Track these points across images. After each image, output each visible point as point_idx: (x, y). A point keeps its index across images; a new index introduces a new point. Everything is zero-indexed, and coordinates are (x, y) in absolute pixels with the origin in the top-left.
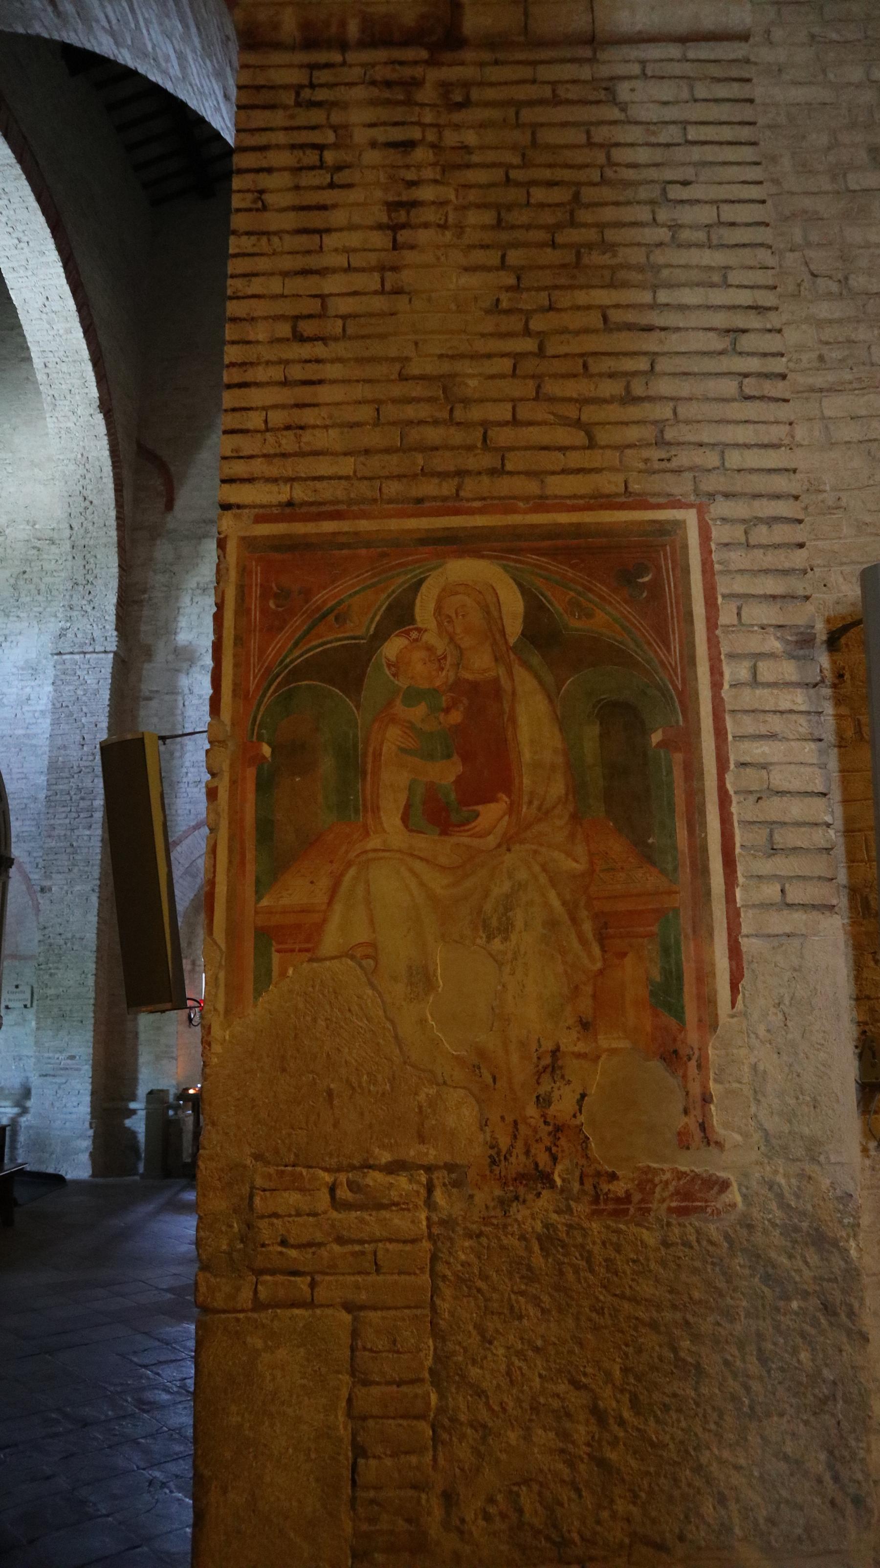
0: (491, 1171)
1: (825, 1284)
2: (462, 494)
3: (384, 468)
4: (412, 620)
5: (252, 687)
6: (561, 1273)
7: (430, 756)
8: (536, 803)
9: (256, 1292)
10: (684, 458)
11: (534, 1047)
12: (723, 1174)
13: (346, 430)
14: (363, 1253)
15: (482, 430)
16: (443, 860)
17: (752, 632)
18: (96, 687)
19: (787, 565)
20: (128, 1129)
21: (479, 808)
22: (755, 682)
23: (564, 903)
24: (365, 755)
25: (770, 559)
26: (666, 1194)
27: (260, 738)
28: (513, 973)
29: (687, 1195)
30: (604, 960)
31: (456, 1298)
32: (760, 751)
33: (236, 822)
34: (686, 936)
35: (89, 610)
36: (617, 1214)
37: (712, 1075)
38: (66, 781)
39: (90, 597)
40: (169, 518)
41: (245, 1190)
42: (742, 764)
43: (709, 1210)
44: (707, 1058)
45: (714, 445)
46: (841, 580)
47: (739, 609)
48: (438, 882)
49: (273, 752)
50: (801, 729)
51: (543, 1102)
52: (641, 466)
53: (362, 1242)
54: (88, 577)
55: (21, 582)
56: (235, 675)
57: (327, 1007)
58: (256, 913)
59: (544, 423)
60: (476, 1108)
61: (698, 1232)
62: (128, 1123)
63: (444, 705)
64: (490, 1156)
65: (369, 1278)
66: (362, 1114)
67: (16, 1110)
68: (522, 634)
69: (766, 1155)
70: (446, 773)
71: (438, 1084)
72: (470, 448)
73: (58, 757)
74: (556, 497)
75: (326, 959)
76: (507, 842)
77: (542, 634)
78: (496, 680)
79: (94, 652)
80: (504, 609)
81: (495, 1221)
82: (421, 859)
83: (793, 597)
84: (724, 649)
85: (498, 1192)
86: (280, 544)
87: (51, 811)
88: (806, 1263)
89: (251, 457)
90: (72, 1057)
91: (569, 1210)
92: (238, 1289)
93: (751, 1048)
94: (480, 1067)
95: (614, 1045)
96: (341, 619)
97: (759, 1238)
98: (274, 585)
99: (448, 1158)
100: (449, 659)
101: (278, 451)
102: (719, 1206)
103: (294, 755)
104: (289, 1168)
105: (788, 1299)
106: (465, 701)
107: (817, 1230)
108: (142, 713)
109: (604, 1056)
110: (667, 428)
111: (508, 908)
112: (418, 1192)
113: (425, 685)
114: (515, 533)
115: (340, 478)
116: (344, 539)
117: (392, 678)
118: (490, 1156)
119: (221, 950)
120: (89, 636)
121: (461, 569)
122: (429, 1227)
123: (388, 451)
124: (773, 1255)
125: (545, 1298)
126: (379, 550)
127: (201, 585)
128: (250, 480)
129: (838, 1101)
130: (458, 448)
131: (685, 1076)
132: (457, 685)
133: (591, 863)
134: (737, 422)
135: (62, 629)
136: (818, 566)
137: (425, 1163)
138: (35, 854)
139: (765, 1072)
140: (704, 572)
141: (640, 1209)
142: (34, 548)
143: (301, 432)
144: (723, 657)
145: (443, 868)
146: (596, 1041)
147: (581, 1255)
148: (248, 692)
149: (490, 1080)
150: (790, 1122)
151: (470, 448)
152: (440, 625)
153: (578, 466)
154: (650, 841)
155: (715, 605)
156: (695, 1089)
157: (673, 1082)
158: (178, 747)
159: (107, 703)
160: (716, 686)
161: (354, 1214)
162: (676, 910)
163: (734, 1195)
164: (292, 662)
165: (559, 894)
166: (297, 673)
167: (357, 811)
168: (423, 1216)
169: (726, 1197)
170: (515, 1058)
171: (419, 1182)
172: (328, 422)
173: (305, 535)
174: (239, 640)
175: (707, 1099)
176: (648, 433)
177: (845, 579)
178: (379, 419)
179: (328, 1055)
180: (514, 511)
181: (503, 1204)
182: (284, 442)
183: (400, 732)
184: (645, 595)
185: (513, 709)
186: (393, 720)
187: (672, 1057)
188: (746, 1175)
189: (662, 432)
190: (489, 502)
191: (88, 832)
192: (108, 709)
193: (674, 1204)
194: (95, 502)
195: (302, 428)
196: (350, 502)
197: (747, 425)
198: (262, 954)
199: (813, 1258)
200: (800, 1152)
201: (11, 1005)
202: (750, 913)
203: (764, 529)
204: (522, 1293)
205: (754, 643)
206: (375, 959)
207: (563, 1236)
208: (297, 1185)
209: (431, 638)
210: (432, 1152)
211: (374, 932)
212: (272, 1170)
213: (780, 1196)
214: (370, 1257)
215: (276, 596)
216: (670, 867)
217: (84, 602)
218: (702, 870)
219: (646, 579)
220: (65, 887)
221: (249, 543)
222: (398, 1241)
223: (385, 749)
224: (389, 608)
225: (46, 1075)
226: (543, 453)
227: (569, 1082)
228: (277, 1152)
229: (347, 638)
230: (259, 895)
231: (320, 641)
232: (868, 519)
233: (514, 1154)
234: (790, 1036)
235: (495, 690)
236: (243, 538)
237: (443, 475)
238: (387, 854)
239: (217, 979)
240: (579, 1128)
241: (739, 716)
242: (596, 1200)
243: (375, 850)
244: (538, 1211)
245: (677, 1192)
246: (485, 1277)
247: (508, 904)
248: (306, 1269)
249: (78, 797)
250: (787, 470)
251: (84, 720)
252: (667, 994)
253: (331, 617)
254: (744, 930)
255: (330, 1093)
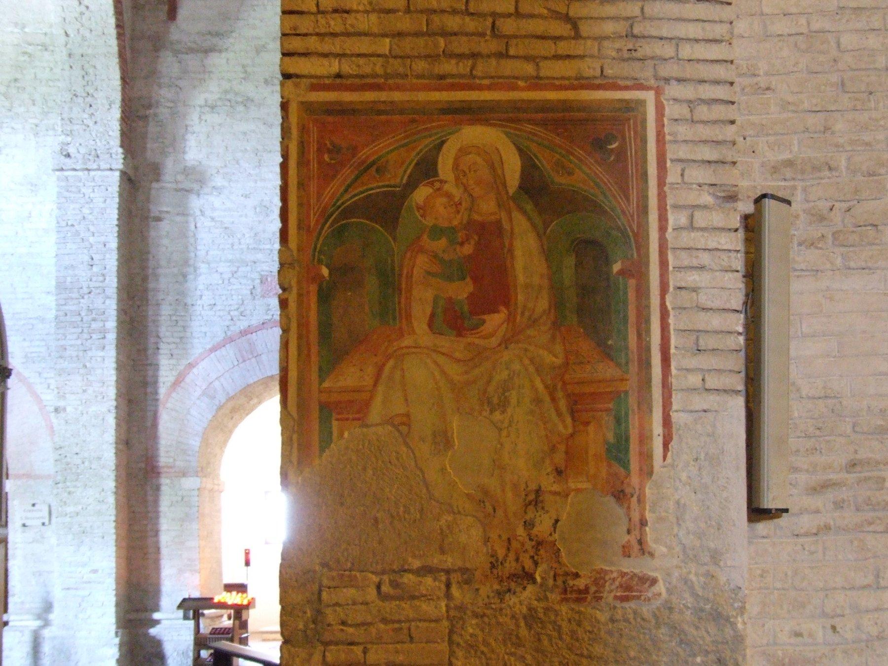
0: (492, 573)
1: (719, 646)
2: (474, 72)
3: (413, 49)
4: (436, 174)
5: (312, 224)
6: (539, 640)
7: (450, 278)
8: (527, 314)
9: (324, 656)
10: (646, 49)
11: (523, 486)
12: (653, 574)
13: (382, 15)
14: (401, 629)
15: (490, 20)
16: (457, 355)
17: (691, 189)
18: (103, 205)
19: (720, 138)
20: (154, 637)
21: (485, 317)
22: (691, 227)
23: (546, 387)
24: (400, 275)
25: (706, 132)
26: (613, 587)
27: (320, 261)
28: (508, 436)
29: (629, 588)
30: (574, 427)
31: (466, 658)
32: (693, 278)
33: (303, 325)
34: (633, 410)
35: (91, 124)
36: (578, 600)
37: (647, 507)
38: (76, 302)
39: (92, 111)
40: (173, 28)
41: (316, 587)
42: (679, 288)
43: (643, 598)
44: (645, 495)
45: (671, 39)
46: (766, 148)
47: (683, 170)
48: (454, 371)
49: (330, 274)
50: (723, 263)
51: (529, 525)
52: (614, 54)
53: (399, 621)
54: (88, 89)
55: (14, 91)
56: (299, 213)
57: (374, 459)
58: (320, 392)
59: (540, 16)
60: (481, 530)
61: (635, 612)
62: (153, 631)
63: (460, 240)
64: (491, 563)
65: (405, 646)
66: (399, 534)
67: (38, 623)
68: (520, 187)
69: (683, 561)
70: (461, 291)
71: (454, 513)
72: (482, 35)
73: (65, 277)
74: (548, 78)
75: (372, 425)
76: (506, 342)
77: (534, 187)
78: (499, 222)
79: (99, 169)
80: (506, 166)
81: (493, 606)
82: (443, 354)
83: (723, 163)
84: (670, 201)
85: (496, 587)
86: (331, 109)
87: (61, 331)
88: (708, 632)
89: (306, 35)
90: (95, 571)
91: (546, 598)
92: (311, 655)
93: (676, 489)
94: (485, 502)
95: (580, 486)
96: (381, 171)
97: (676, 616)
98: (328, 142)
99: (459, 563)
100: (464, 204)
101: (327, 30)
102: (650, 595)
103: (346, 273)
104: (347, 573)
105: (695, 655)
106: (476, 237)
107: (716, 610)
108: (153, 233)
109: (572, 494)
110: (636, 25)
111: (506, 389)
112: (440, 588)
113: (445, 224)
114: (517, 107)
115: (379, 56)
116: (382, 107)
117: (420, 218)
118: (491, 563)
119: (293, 419)
120: (93, 153)
121: (474, 134)
122: (447, 611)
123: (417, 34)
124: (686, 627)
125: (529, 657)
126: (411, 116)
127: (210, 102)
128: (305, 55)
129: (734, 525)
130: (473, 34)
131: (629, 508)
132: (470, 222)
133: (567, 358)
134: (690, 21)
135: (63, 143)
136: (750, 136)
137: (445, 567)
138: (45, 375)
139: (685, 504)
140: (658, 141)
141: (595, 597)
142: (25, 53)
143: (346, 15)
144: (668, 207)
145: (458, 361)
146: (567, 483)
147: (554, 628)
148: (309, 226)
149: (490, 510)
150: (700, 538)
151: (482, 35)
152: (457, 179)
153: (565, 53)
154: (610, 342)
155: (665, 168)
156: (636, 516)
157: (620, 511)
158: (191, 270)
159: (116, 222)
160: (663, 229)
161: (394, 603)
162: (626, 392)
163: (661, 587)
164: (343, 203)
165: (542, 380)
166: (348, 212)
167: (394, 319)
168: (443, 604)
169: (656, 589)
170: (509, 495)
171: (441, 581)
172: (368, 8)
173: (351, 102)
174: (301, 185)
175: (643, 523)
176: (621, 27)
177: (769, 147)
178: (409, 7)
179: (374, 493)
180: (514, 88)
181: (500, 594)
182: (332, 23)
183: (426, 260)
184: (612, 159)
185: (511, 245)
186: (421, 250)
187: (620, 496)
188: (668, 575)
189: (631, 26)
190: (496, 80)
191: (102, 354)
192: (117, 229)
193: (618, 594)
194: (92, 7)
195: (347, 12)
196: (387, 76)
197: (697, 23)
198: (325, 421)
199: (713, 630)
200: (707, 559)
201: (28, 523)
202: (680, 395)
203: (704, 108)
204: (512, 654)
205: (692, 198)
206: (409, 426)
207: (541, 615)
208: (352, 583)
209: (449, 187)
210: (450, 560)
211: (408, 406)
212: (334, 574)
213: (692, 588)
214: (406, 631)
215: (329, 151)
216: (623, 361)
217: (86, 116)
218: (645, 364)
219: (614, 146)
220: (80, 408)
221: (308, 107)
222: (425, 621)
223: (415, 272)
224: (417, 164)
225: (68, 589)
226: (539, 42)
227: (547, 512)
228: (338, 561)
229: (388, 186)
230: (322, 379)
231: (365, 188)
232: (790, 99)
233: (508, 561)
234: (703, 481)
235: (497, 229)
236: (302, 103)
237: (461, 56)
238: (418, 350)
239: (291, 440)
240: (554, 543)
241: (678, 252)
242: (565, 591)
243: (407, 347)
244: (525, 597)
245: (621, 586)
246: (486, 643)
247: (505, 387)
248: (361, 641)
249: (90, 318)
250: (726, 61)
251: (92, 239)
252: (618, 451)
253: (374, 169)
254: (674, 407)
255: (376, 520)
